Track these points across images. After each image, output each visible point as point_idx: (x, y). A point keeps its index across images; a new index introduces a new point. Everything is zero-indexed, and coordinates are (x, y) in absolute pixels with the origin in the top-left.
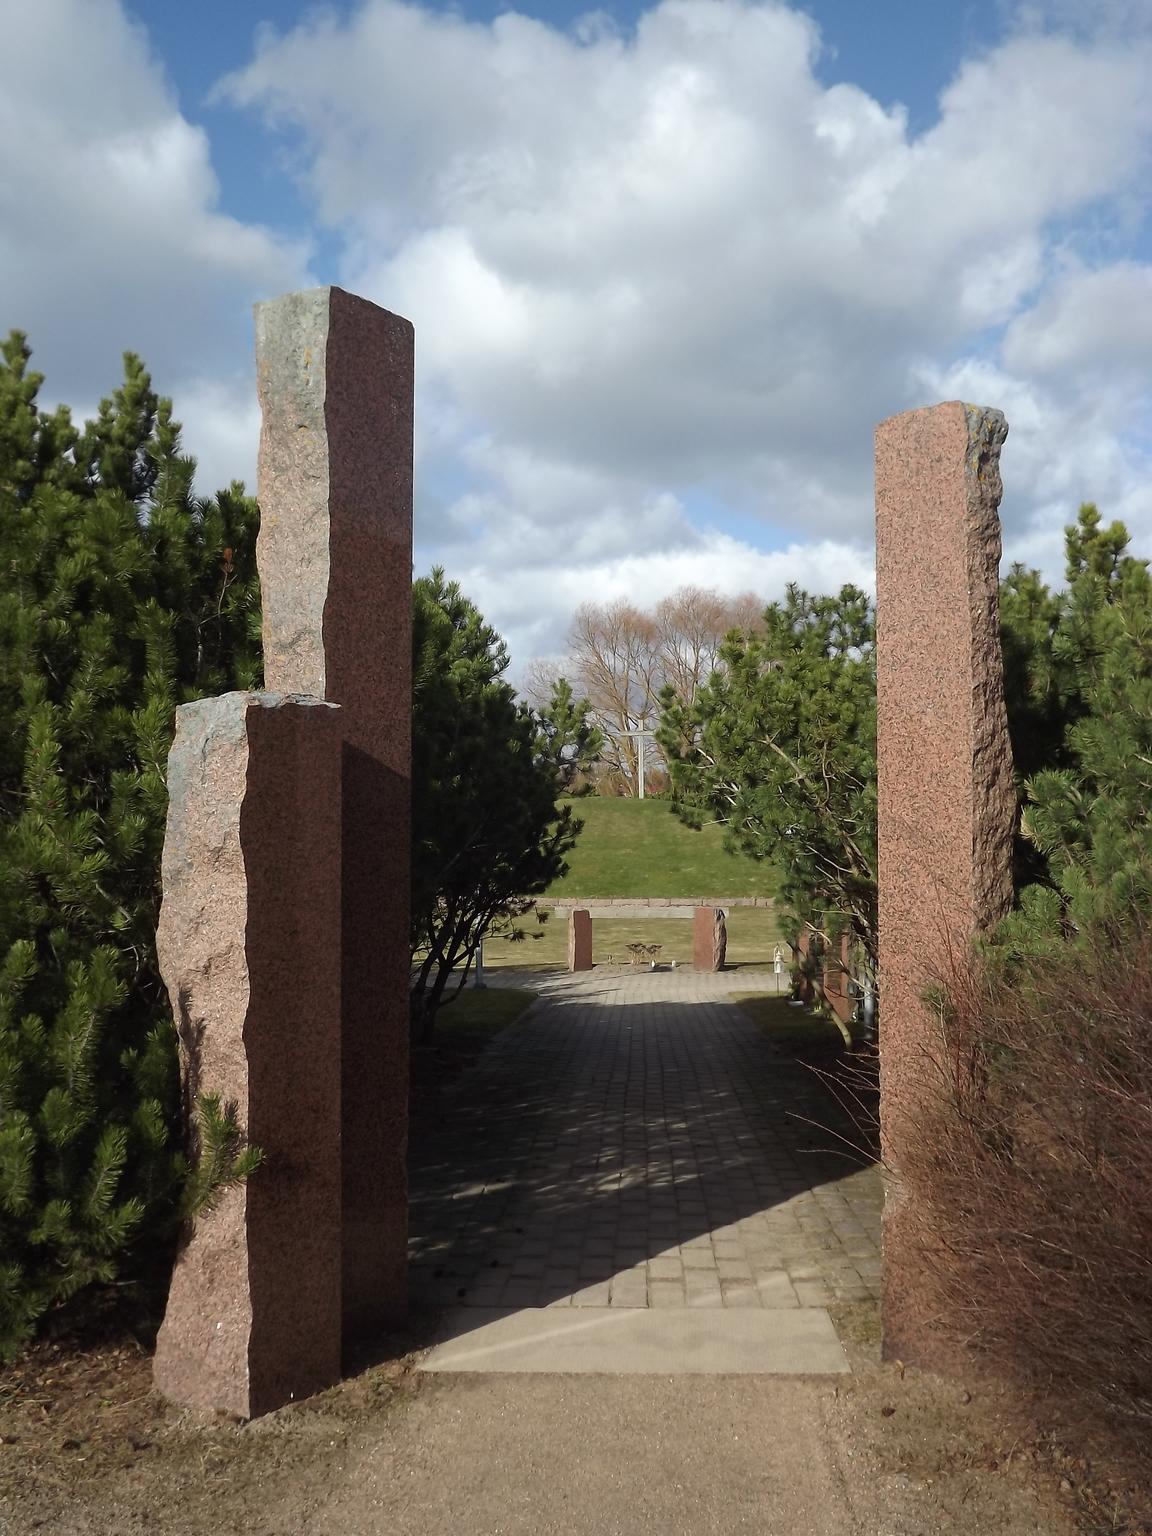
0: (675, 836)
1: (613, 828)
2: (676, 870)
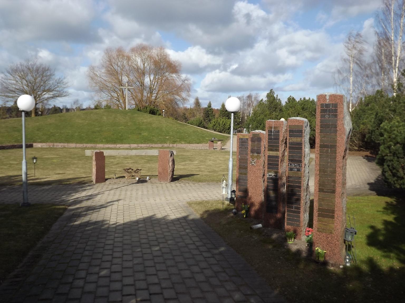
0: (139, 122)
1: (117, 119)
2: (140, 134)
